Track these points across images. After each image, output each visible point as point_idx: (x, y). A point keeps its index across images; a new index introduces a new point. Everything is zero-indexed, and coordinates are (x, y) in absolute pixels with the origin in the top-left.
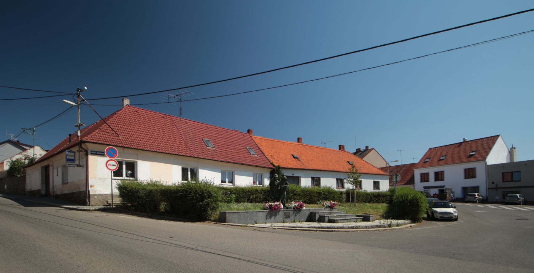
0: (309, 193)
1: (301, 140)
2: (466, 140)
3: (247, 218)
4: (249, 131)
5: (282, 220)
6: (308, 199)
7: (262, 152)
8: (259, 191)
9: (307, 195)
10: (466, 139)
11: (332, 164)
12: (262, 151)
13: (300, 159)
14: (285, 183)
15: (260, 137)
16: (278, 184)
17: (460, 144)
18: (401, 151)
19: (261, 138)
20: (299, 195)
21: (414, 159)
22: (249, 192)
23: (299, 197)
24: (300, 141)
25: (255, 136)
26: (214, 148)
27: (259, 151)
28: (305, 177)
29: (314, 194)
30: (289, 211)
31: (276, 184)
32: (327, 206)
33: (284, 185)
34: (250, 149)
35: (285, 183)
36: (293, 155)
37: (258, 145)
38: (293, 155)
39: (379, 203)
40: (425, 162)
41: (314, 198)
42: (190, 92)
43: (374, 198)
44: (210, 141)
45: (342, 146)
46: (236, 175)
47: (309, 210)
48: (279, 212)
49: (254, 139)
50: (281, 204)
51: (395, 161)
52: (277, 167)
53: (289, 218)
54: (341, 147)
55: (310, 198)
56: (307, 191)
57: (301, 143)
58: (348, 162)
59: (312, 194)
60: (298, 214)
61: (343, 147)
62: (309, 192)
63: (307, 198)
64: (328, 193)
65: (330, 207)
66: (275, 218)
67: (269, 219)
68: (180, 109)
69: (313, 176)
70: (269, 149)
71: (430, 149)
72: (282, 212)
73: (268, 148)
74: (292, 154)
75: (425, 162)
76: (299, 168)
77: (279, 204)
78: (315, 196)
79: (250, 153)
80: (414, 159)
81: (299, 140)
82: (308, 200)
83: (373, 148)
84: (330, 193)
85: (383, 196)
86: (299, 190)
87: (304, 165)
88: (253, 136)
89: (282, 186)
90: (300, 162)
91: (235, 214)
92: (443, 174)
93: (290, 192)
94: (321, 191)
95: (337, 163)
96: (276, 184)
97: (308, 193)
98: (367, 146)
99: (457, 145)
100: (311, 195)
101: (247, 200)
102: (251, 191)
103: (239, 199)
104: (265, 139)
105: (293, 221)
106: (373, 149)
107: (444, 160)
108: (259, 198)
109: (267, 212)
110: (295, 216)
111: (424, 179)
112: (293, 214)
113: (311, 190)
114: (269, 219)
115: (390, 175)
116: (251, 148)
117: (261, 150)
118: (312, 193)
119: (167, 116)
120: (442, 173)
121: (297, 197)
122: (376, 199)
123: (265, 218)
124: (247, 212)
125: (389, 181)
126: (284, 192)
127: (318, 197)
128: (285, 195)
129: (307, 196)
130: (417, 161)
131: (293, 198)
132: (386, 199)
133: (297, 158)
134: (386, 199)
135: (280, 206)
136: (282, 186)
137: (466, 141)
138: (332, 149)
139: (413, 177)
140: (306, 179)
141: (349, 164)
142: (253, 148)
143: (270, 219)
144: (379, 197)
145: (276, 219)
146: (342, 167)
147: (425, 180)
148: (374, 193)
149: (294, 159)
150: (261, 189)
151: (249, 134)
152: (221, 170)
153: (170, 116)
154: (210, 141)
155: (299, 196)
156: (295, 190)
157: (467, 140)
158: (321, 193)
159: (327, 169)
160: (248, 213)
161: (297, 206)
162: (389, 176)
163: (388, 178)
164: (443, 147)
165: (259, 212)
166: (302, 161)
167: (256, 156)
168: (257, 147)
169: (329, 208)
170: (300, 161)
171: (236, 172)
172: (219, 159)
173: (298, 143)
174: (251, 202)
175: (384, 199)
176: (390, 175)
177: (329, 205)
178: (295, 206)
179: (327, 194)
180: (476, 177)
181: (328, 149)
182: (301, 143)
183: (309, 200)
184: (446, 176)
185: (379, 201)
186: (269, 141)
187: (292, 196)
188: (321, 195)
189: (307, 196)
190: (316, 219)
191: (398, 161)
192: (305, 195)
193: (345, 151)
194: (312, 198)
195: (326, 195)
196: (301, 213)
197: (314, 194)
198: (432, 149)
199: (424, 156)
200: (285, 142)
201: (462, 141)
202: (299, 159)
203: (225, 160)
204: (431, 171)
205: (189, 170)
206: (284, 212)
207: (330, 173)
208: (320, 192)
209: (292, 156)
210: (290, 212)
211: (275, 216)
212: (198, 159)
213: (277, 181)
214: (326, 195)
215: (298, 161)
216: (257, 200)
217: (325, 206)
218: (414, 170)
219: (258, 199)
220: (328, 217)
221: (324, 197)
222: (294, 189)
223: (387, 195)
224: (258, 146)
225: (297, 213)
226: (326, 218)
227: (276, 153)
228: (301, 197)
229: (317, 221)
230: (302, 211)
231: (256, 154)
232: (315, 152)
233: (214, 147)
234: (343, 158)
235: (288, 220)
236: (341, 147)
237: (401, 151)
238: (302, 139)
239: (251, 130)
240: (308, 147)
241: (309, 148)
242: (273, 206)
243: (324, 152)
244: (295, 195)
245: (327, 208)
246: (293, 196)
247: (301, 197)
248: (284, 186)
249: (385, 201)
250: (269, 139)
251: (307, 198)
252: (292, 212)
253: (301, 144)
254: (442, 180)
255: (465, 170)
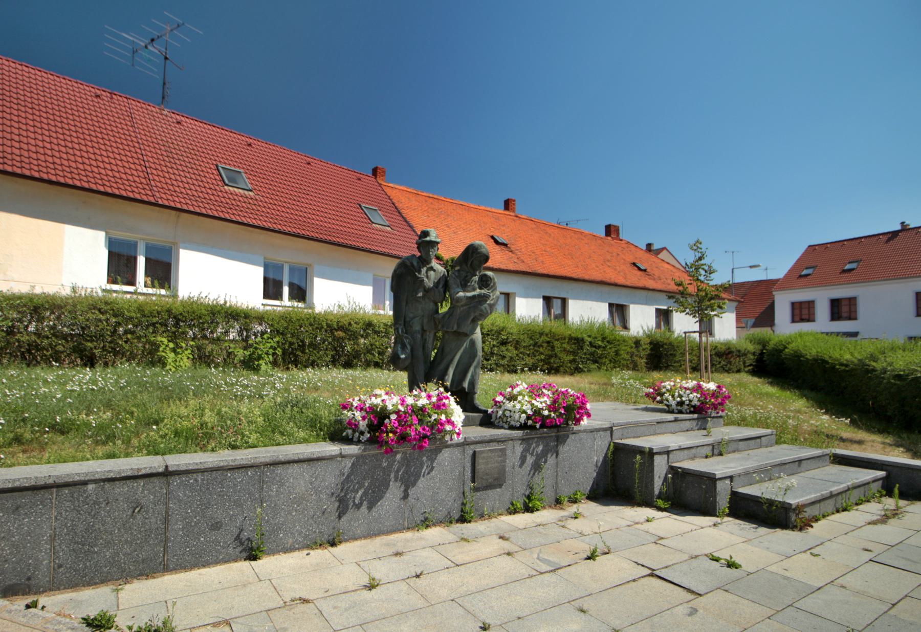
0: (548, 340)
1: (514, 204)
2: (908, 225)
3: (166, 521)
4: (375, 172)
5: (457, 505)
6: (543, 357)
7: (406, 222)
8: (377, 329)
9: (539, 347)
10: (907, 222)
11: (597, 267)
12: (408, 219)
13: (513, 247)
14: (476, 278)
15: (405, 189)
16: (436, 285)
17: (894, 235)
18: (733, 252)
19: (409, 190)
20: (517, 345)
21: (766, 269)
22: (341, 328)
23: (515, 352)
24: (510, 207)
25: (392, 185)
26: (251, 193)
27: (409, 232)
28: (526, 296)
29: (562, 344)
30: (501, 446)
31: (429, 283)
32: (681, 403)
33: (474, 290)
34: (372, 211)
35: (476, 278)
36: (493, 237)
37: (396, 205)
38: (493, 237)
39: (728, 371)
40: (801, 276)
41: (561, 355)
42: (183, 24)
43: (718, 359)
44: (243, 174)
45: (615, 226)
46: (319, 277)
47: (605, 430)
48: (438, 451)
49: (388, 190)
50: (452, 403)
51: (751, 267)
52: (447, 261)
53: (500, 486)
54: (612, 229)
55: (550, 357)
56: (541, 334)
57: (514, 211)
58: (634, 264)
59: (557, 344)
60: (551, 460)
61: (617, 229)
62: (547, 335)
63: (542, 353)
64: (603, 339)
65: (695, 410)
66: (406, 496)
67: (358, 506)
68: (164, 84)
69: (547, 294)
70: (428, 216)
71: (809, 246)
72: (457, 452)
73: (426, 214)
74: (491, 234)
75: (801, 276)
76: (512, 269)
77: (439, 406)
78: (565, 350)
79: (369, 219)
80: (766, 269)
81: (508, 205)
82: (542, 360)
83: (663, 246)
84: (608, 342)
85: (738, 354)
86: (515, 331)
87: (523, 262)
88: (385, 184)
89: (461, 294)
90: (513, 255)
91: (24, 499)
92: (855, 305)
93: (488, 335)
94: (585, 336)
95: (608, 264)
96: (429, 283)
97: (544, 338)
98: (650, 242)
99: (886, 237)
100: (553, 347)
101: (333, 356)
102: (350, 324)
103: (299, 353)
104: (418, 194)
105: (520, 505)
106: (664, 248)
107: (854, 272)
108: (379, 353)
109: (348, 463)
110: (537, 467)
111: (801, 314)
112: (523, 459)
113: (553, 330)
114: (364, 508)
115: (739, 301)
116: (376, 208)
117: (403, 217)
118: (558, 340)
119: (114, 96)
120: (852, 301)
121: (510, 352)
122: (723, 363)
123: (332, 506)
124: (167, 473)
125: (737, 315)
126: (473, 331)
127: (574, 353)
128: (473, 343)
129: (541, 350)
130: (778, 272)
131: (497, 354)
132: (744, 363)
133: (505, 245)
134: (744, 363)
135: (443, 417)
136: (461, 294)
137: (908, 227)
138: (591, 232)
139: (772, 307)
140: (530, 300)
141: (636, 268)
142: (380, 210)
143: (370, 508)
144: (730, 356)
145: (411, 499)
146: (622, 274)
147: (804, 317)
148: (719, 346)
149: (497, 247)
150: (384, 321)
151: (376, 178)
152: (265, 258)
153: (127, 98)
154: (243, 174)
155: (516, 348)
156: (503, 329)
157: (911, 226)
158: (583, 340)
159: (587, 277)
160: (176, 481)
161: (546, 413)
162: (735, 304)
163: (734, 309)
164: (829, 246)
165: (279, 470)
166: (517, 252)
167: (389, 229)
168: (394, 209)
169: (696, 416)
170: (511, 251)
171: (317, 268)
172: (256, 223)
173: (507, 212)
174: (348, 365)
175: (741, 363)
176: (739, 301)
177: (696, 402)
178: (537, 412)
179: (600, 343)
180: (858, 317)
181: (582, 233)
182: (514, 211)
183: (546, 361)
184: (862, 309)
185: (729, 365)
186: (431, 200)
187: (494, 346)
188: (582, 348)
189: (541, 350)
190: (657, 492)
191: (758, 266)
192: (535, 345)
193: (621, 240)
194: (556, 356)
195: (595, 347)
196: (564, 449)
197: (562, 344)
198: (817, 248)
199: (795, 263)
200: (472, 206)
201: (899, 227)
202: (509, 248)
203: (279, 227)
204: (822, 297)
205: (141, 248)
206: (469, 451)
207: (594, 286)
208: (580, 336)
209: (490, 238)
210: (503, 451)
211: (408, 482)
212: (174, 212)
213: (432, 269)
214: (595, 347)
215: (507, 252)
216: (369, 357)
217: (673, 403)
218: (774, 293)
219: (374, 356)
220: (728, 482)
221: (592, 354)
222: (502, 325)
223: (748, 352)
224: (396, 208)
225: (544, 454)
226: (720, 485)
227: (448, 227)
228: (521, 353)
229: (660, 503)
230: (572, 437)
231: (387, 223)
232: (550, 235)
233: (251, 191)
234: (620, 254)
235: (492, 498)
236: (610, 230)
237: (733, 252)
238: (516, 203)
239: (380, 169)
240: (531, 222)
241: (534, 226)
242: (393, 417)
243: (571, 238)
244: (504, 343)
245: (680, 412)
246: (496, 348)
247: (521, 353)
248: (469, 294)
249: (742, 367)
250: (431, 195)
251: (542, 353)
252: (519, 449)
253: (511, 214)
254: (852, 316)
255: (793, 304)
